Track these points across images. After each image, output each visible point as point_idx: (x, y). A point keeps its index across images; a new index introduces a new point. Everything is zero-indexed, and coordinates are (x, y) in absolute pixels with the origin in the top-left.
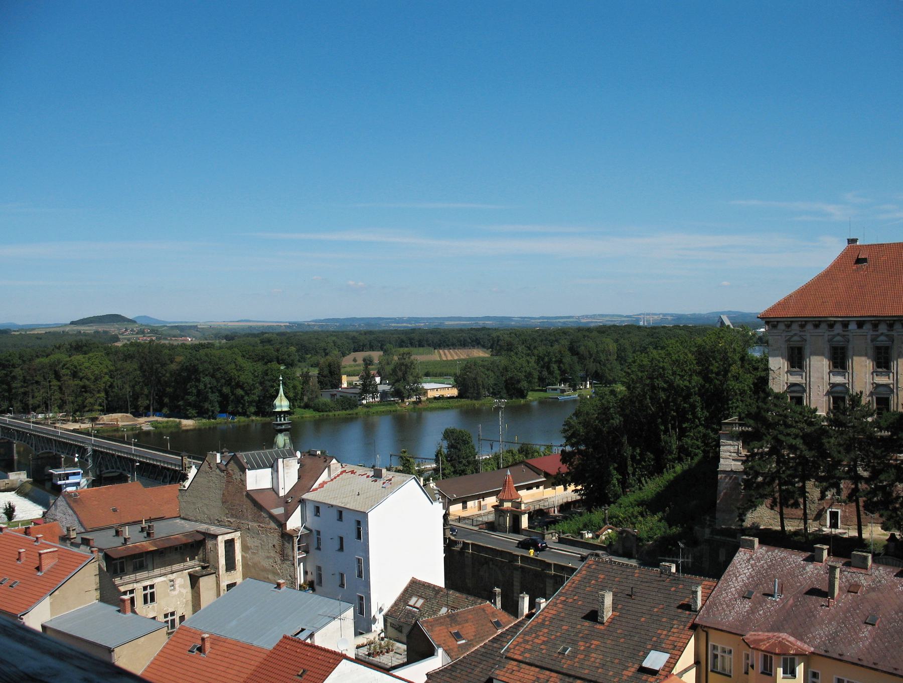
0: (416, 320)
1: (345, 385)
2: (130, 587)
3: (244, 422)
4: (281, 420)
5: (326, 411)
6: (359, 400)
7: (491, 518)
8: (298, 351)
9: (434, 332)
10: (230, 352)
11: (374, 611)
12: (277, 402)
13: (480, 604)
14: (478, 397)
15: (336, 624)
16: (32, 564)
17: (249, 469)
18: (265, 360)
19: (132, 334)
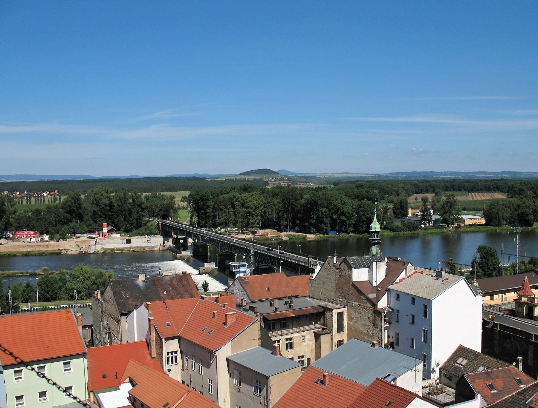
1: (410, 215)
2: (278, 338)
3: (346, 237)
4: (374, 237)
5: (398, 232)
6: (420, 225)
7: (513, 306)
8: (379, 193)
9: (468, 181)
10: (338, 193)
11: (433, 365)
12: (372, 225)
13: (507, 366)
14: (499, 225)
15: (410, 373)
16: (221, 321)
17: (354, 268)
18: (360, 198)
19: (276, 181)
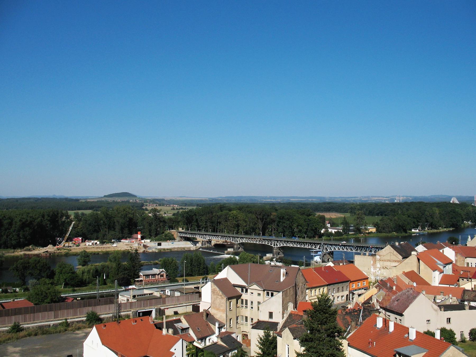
0: (274, 198)
